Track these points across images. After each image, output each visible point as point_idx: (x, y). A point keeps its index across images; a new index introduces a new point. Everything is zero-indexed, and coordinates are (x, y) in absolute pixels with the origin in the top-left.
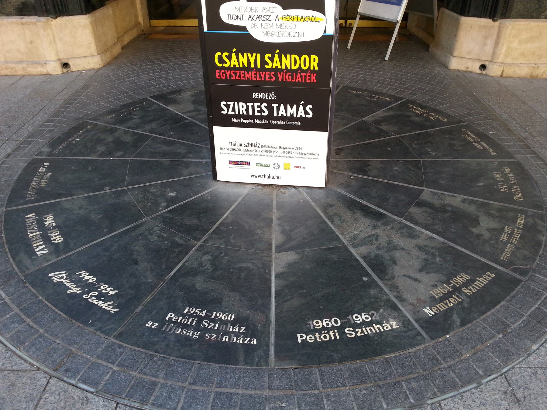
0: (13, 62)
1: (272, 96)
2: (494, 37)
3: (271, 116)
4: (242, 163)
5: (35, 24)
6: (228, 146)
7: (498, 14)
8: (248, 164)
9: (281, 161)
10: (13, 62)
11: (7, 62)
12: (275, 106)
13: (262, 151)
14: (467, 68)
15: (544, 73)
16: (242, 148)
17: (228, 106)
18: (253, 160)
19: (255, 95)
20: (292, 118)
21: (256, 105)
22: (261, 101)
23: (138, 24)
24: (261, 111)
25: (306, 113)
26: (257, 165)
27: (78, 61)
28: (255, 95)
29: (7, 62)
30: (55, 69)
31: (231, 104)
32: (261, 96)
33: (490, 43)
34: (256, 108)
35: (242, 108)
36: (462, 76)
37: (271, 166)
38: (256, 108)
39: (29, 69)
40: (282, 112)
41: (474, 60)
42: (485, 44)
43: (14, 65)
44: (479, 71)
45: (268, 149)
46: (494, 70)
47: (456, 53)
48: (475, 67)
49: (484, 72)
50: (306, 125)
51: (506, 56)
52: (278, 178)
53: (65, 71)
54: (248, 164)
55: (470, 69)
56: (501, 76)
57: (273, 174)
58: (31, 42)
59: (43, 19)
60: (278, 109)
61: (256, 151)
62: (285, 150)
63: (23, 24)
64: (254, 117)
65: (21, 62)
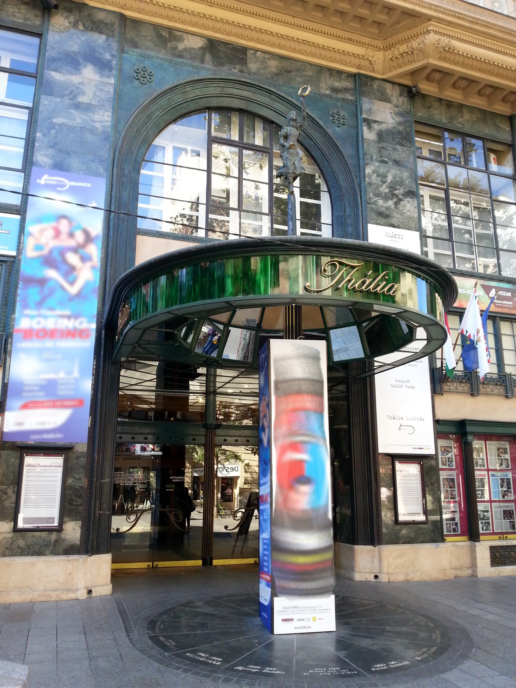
0: (50, 590)
2: (378, 557)
5: (78, 560)
6: (281, 609)
7: (376, 543)
8: (292, 620)
10: (50, 590)
11: (45, 590)
13: (301, 611)
14: (366, 579)
16: (290, 610)
18: (295, 617)
26: (298, 620)
27: (98, 589)
30: (82, 595)
33: (376, 560)
36: (365, 584)
37: (306, 619)
39: (62, 595)
41: (369, 573)
42: (373, 562)
43: (51, 593)
44: (374, 580)
46: (384, 578)
47: (357, 569)
48: (371, 578)
49: (378, 580)
51: (388, 568)
52: (310, 627)
53: (88, 596)
54: (292, 620)
55: (368, 579)
57: (307, 626)
58: (70, 574)
59: (84, 556)
61: (297, 611)
63: (68, 560)
65: (57, 590)
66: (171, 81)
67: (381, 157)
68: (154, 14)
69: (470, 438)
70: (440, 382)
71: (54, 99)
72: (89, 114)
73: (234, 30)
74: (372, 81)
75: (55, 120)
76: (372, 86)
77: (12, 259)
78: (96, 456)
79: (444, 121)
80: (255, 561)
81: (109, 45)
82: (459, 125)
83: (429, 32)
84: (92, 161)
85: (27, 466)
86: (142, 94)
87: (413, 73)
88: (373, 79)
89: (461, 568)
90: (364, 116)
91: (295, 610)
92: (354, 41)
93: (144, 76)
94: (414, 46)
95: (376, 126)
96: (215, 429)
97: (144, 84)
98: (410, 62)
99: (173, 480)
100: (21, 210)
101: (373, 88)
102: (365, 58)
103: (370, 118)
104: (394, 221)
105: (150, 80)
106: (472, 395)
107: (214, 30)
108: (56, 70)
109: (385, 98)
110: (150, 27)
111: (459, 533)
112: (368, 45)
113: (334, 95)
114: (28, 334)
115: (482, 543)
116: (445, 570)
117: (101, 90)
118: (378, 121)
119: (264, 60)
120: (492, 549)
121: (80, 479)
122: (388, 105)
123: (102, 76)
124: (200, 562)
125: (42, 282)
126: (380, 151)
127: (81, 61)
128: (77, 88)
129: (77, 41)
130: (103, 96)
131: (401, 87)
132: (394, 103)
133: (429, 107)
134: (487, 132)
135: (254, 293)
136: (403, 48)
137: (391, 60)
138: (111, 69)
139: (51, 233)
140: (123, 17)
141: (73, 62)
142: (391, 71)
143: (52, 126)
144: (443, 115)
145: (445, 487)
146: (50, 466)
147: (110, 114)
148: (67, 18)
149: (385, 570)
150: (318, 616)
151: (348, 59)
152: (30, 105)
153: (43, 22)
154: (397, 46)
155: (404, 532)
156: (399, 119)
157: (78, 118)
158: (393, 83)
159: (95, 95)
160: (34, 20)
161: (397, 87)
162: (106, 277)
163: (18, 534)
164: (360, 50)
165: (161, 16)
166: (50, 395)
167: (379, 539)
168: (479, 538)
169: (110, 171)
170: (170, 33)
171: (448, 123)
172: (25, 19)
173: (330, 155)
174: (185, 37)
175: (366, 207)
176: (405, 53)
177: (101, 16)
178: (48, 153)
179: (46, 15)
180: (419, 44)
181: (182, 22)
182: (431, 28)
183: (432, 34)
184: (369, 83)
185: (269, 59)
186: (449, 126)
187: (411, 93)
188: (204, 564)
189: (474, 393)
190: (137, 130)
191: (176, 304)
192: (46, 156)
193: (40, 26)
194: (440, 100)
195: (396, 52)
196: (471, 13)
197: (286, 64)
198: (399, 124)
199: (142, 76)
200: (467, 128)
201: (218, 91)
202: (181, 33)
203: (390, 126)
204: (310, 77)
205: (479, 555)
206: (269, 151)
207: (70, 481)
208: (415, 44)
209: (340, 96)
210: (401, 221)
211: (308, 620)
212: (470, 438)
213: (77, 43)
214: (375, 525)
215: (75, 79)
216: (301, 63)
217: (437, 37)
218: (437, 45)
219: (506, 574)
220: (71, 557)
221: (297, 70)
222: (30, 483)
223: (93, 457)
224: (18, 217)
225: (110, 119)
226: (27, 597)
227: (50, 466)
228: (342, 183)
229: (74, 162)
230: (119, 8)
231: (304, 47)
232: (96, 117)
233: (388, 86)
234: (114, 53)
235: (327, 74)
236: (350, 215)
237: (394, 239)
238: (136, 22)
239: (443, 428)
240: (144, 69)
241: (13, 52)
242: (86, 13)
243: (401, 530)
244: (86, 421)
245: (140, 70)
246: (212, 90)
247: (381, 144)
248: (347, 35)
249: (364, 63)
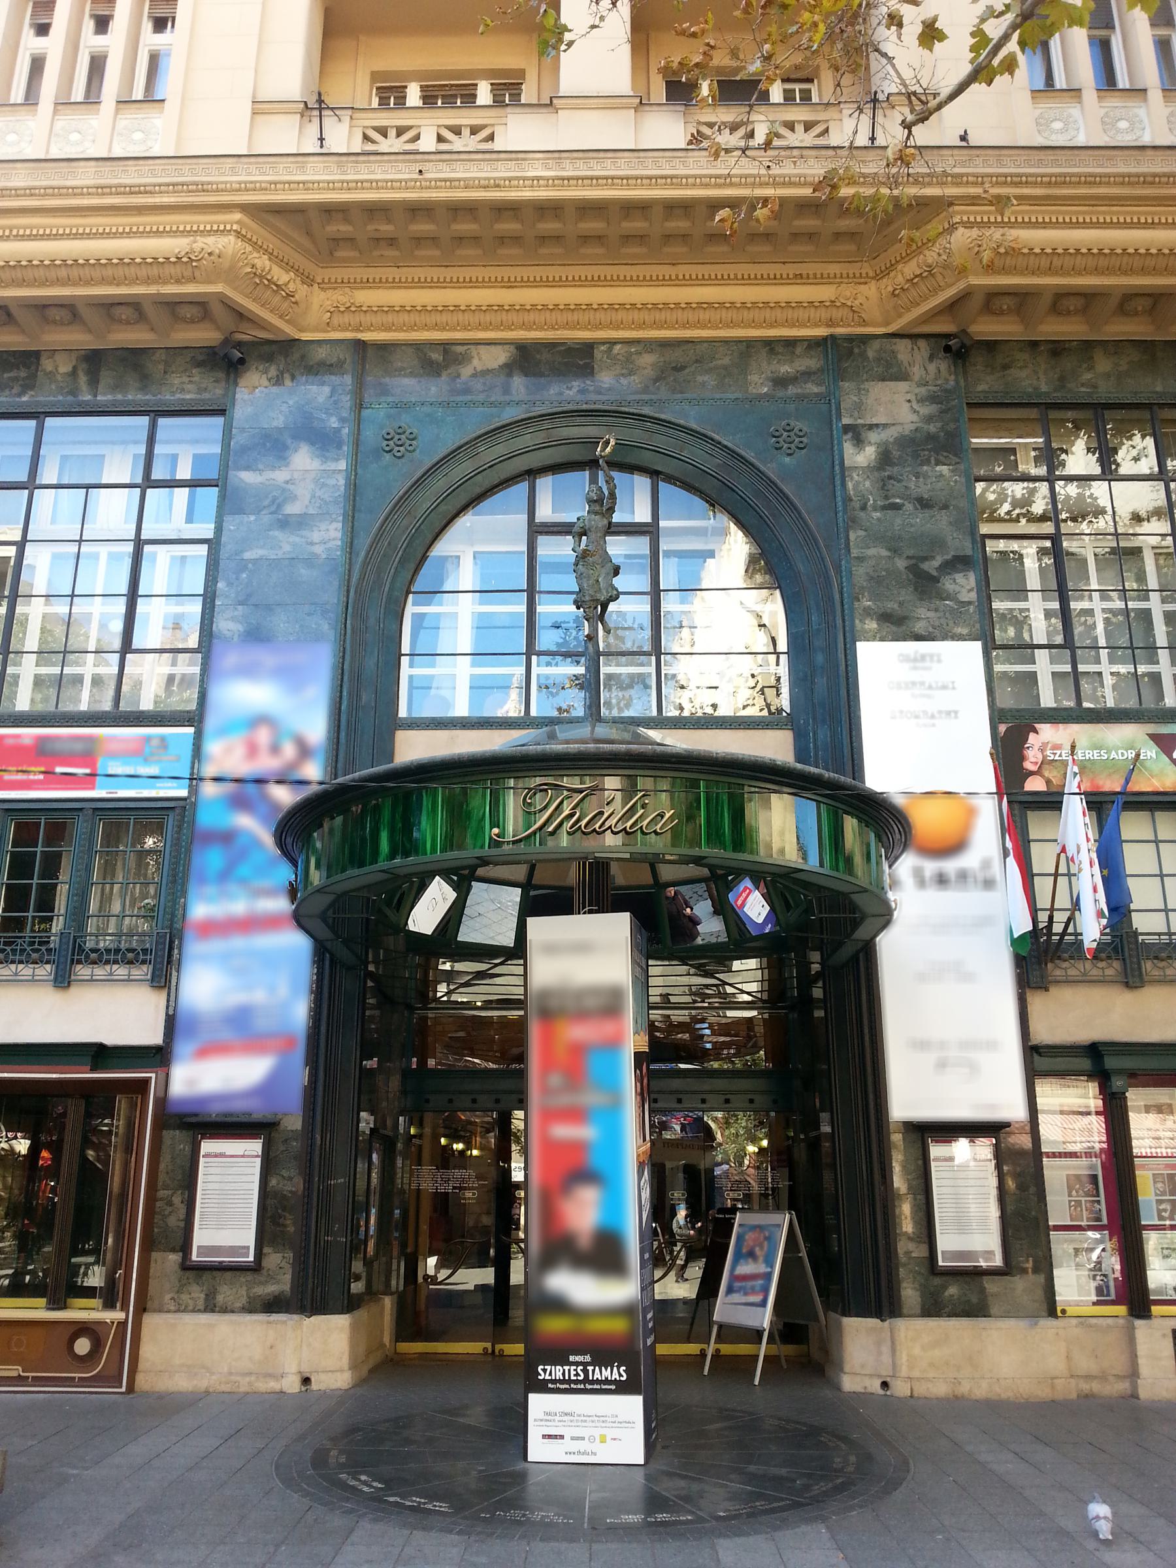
1: (588, 1358)
2: (889, 1343)
3: (586, 1380)
4: (555, 1437)
5: (284, 1322)
6: (542, 1416)
7: (885, 1309)
8: (562, 1437)
9: (597, 1433)
11: (231, 1374)
12: (590, 1368)
15: (970, 1391)
16: (557, 1418)
17: (545, 1370)
18: (567, 1433)
19: (572, 1358)
20: (607, 1381)
21: (573, 1368)
22: (577, 1364)
23: (382, 1345)
24: (577, 1375)
25: (620, 1375)
26: (573, 1438)
27: (323, 1377)
28: (572, 1358)
29: (231, 1374)
30: (291, 1384)
31: (548, 1368)
32: (579, 1358)
33: (886, 1349)
34: (572, 1372)
35: (558, 1372)
36: (863, 1397)
38: (572, 1372)
40: (597, 1376)
41: (871, 1376)
42: (880, 1353)
43: (238, 1378)
44: (881, 1392)
45: (585, 1419)
46: (900, 1389)
47: (847, 1368)
48: (875, 1386)
50: (622, 1388)
51: (911, 1368)
53: (304, 1389)
54: (562, 1437)
55: (870, 1390)
56: (911, 1396)
59: (295, 1317)
60: (593, 1371)
62: (601, 1419)
63: (269, 1323)
64: (570, 1381)
66: (450, 439)
67: (886, 497)
68: (413, 327)
69: (1119, 1083)
70: (1040, 964)
71: (245, 518)
72: (304, 533)
73: (562, 318)
74: (864, 343)
75: (247, 555)
76: (863, 355)
77: (182, 803)
78: (318, 1137)
79: (1044, 388)
81: (335, 403)
82: (1083, 389)
83: (952, 228)
84: (309, 614)
85: (206, 1156)
86: (394, 477)
87: (952, 307)
88: (865, 339)
89: (1103, 1377)
90: (846, 421)
91: (565, 1418)
92: (808, 278)
93: (400, 443)
94: (930, 261)
95: (873, 436)
97: (399, 458)
98: (934, 292)
100: (195, 719)
101: (866, 358)
102: (838, 304)
103: (860, 421)
104: (920, 627)
105: (410, 448)
106: (1127, 985)
107: (524, 326)
108: (247, 468)
109: (893, 372)
110: (410, 350)
111: (1113, 1297)
112: (848, 277)
113: (780, 393)
114: (210, 928)
115: (1155, 1322)
116: (1052, 1378)
117: (324, 485)
118: (877, 425)
119: (629, 359)
121: (290, 1179)
122: (903, 386)
123: (325, 459)
125: (227, 837)
126: (884, 485)
127: (289, 441)
128: (284, 490)
129: (283, 408)
130: (326, 497)
131: (932, 340)
132: (916, 378)
133: (1005, 367)
134: (1159, 389)
135: (417, 854)
136: (911, 269)
137: (893, 294)
138: (339, 446)
139: (240, 751)
140: (360, 345)
141: (274, 447)
142: (900, 316)
143: (243, 566)
144: (1042, 376)
145: (1074, 1193)
146: (243, 1156)
147: (340, 525)
148: (266, 372)
149: (904, 1371)
150: (610, 1433)
151: (802, 314)
152: (210, 535)
153: (227, 389)
154: (900, 267)
155: (953, 1291)
156: (927, 410)
157: (286, 543)
158: (913, 337)
159: (313, 496)
160: (214, 392)
161: (922, 343)
163: (188, 1273)
164: (825, 293)
165: (426, 327)
166: (239, 1031)
167: (891, 1304)
168: (1150, 1311)
169: (340, 626)
170: (446, 352)
171: (1055, 390)
172: (201, 390)
173: (773, 515)
174: (474, 353)
175: (852, 609)
176: (916, 276)
177: (322, 353)
178: (236, 613)
179: (232, 376)
180: (939, 255)
181: (465, 329)
182: (957, 219)
183: (961, 230)
184: (856, 350)
185: (639, 353)
186: (1059, 397)
187: (957, 350)
189: (1132, 979)
190: (389, 544)
192: (233, 619)
193: (224, 395)
194: (1034, 344)
195: (900, 279)
196: (1046, 166)
197: (677, 356)
198: (929, 419)
199: (397, 443)
200: (1106, 391)
201: (540, 438)
202: (466, 347)
203: (908, 429)
204: (725, 368)
205: (1142, 1349)
206: (651, 529)
207: (273, 1182)
208: (931, 256)
209: (792, 390)
210: (937, 623)
211: (592, 1439)
212: (1119, 1083)
213: (281, 412)
214: (883, 1275)
215: (280, 476)
216: (705, 345)
217: (975, 232)
218: (977, 249)
220: (275, 1317)
221: (697, 361)
222: (210, 1186)
223: (313, 1138)
224: (191, 730)
225: (339, 535)
226: (202, 1383)
227: (243, 1156)
228: (801, 567)
229: (280, 622)
230: (352, 331)
231: (704, 316)
232: (316, 536)
233: (902, 346)
234: (345, 414)
235: (764, 352)
236: (818, 630)
237: (919, 665)
238: (384, 348)
239: (1041, 1060)
240: (400, 431)
241: (196, 441)
242: (296, 356)
243: (945, 1288)
244: (300, 1075)
245: (392, 433)
246: (528, 439)
247: (885, 470)
248: (791, 269)
249: (837, 314)
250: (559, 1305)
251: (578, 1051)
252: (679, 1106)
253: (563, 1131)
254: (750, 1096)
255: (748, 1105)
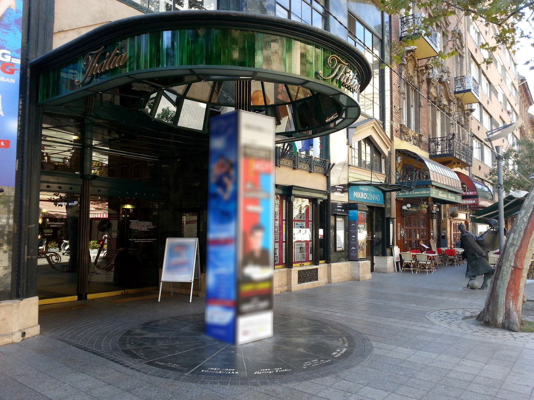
58: (3, 320)
80: (122, 293)
96: (91, 180)
99: (51, 226)
120: (299, 272)
124: (75, 298)
162: (29, 9)
188: (79, 299)
191: (201, 63)
219: (305, 288)
250: (249, 280)
251: (257, 173)
252: (99, 189)
253: (251, 208)
254: (71, 186)
255: (58, 189)
